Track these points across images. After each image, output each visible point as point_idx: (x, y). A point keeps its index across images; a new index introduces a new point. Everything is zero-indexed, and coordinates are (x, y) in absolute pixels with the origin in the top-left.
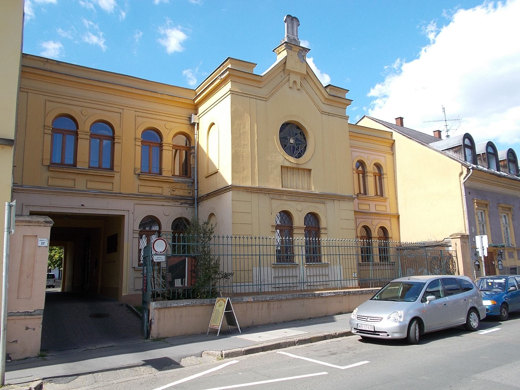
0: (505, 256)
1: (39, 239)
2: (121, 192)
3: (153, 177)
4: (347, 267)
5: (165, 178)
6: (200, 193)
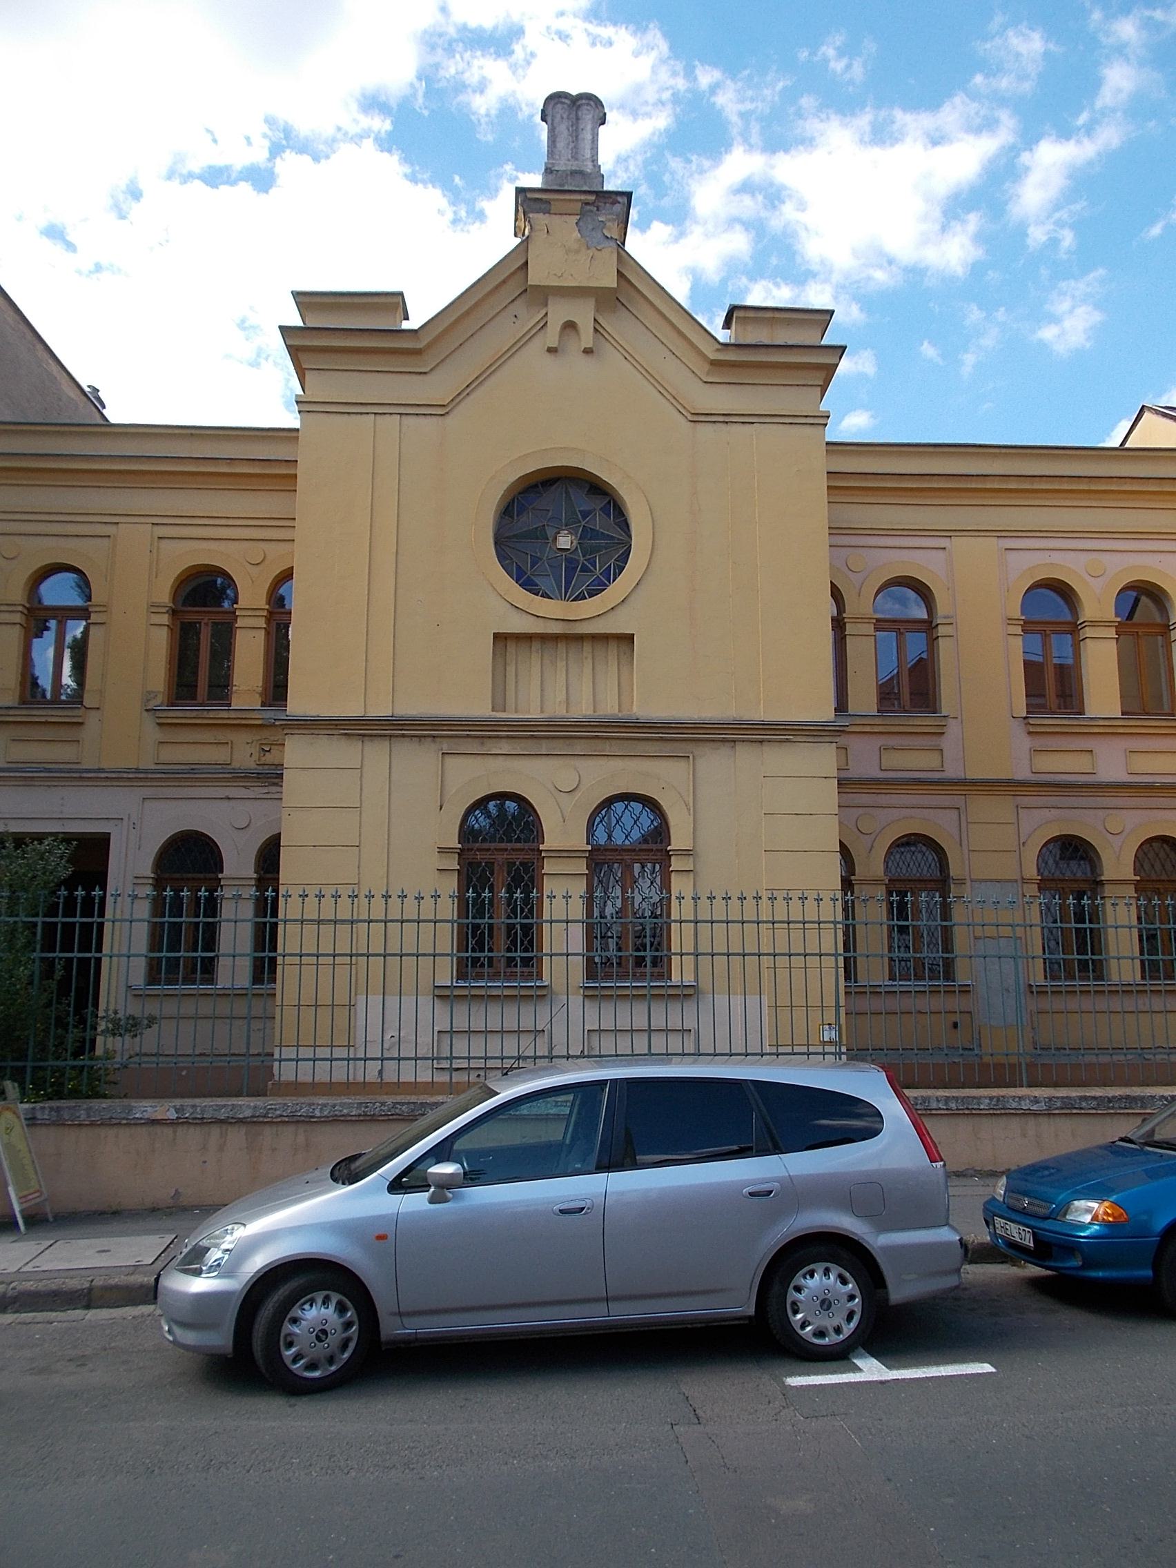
2: (104, 765)
3: (194, 714)
5: (239, 715)
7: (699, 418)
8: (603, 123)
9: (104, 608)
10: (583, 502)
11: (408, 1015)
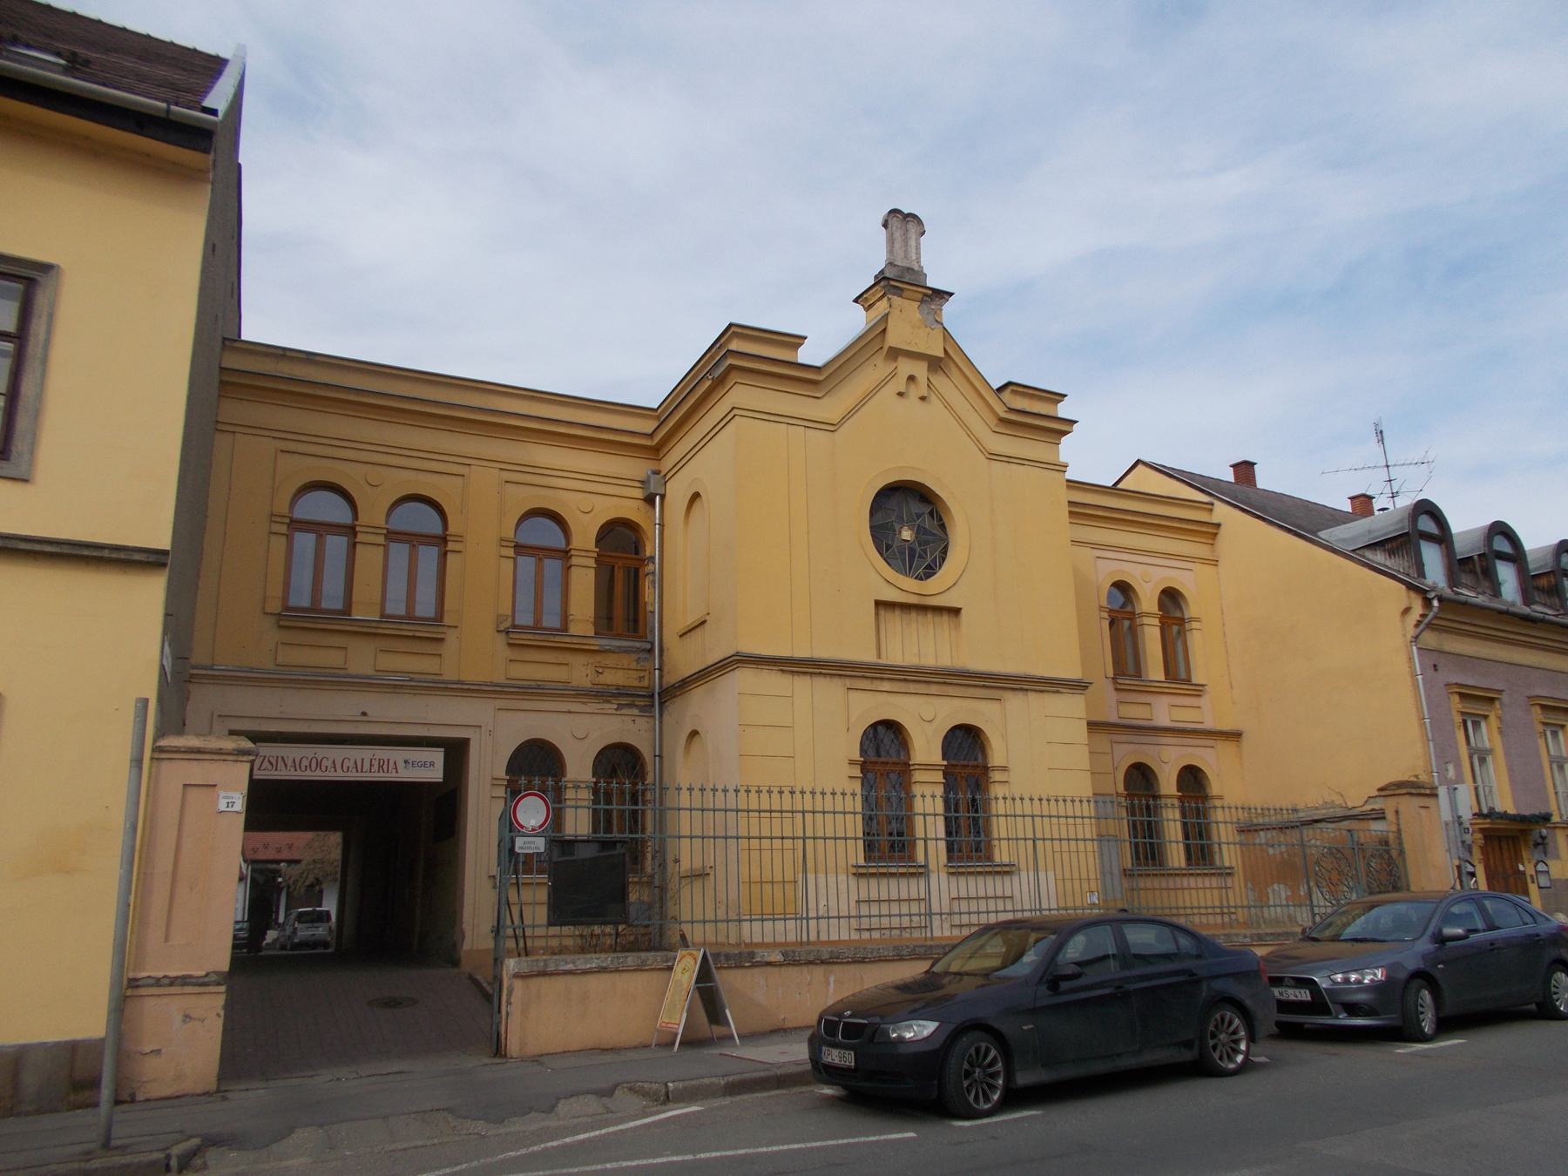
0: (1556, 848)
1: (222, 794)
4: (1067, 875)
5: (575, 640)
6: (665, 679)
7: (993, 457)
8: (923, 233)
9: (460, 539)
10: (916, 507)
11: (832, 885)
